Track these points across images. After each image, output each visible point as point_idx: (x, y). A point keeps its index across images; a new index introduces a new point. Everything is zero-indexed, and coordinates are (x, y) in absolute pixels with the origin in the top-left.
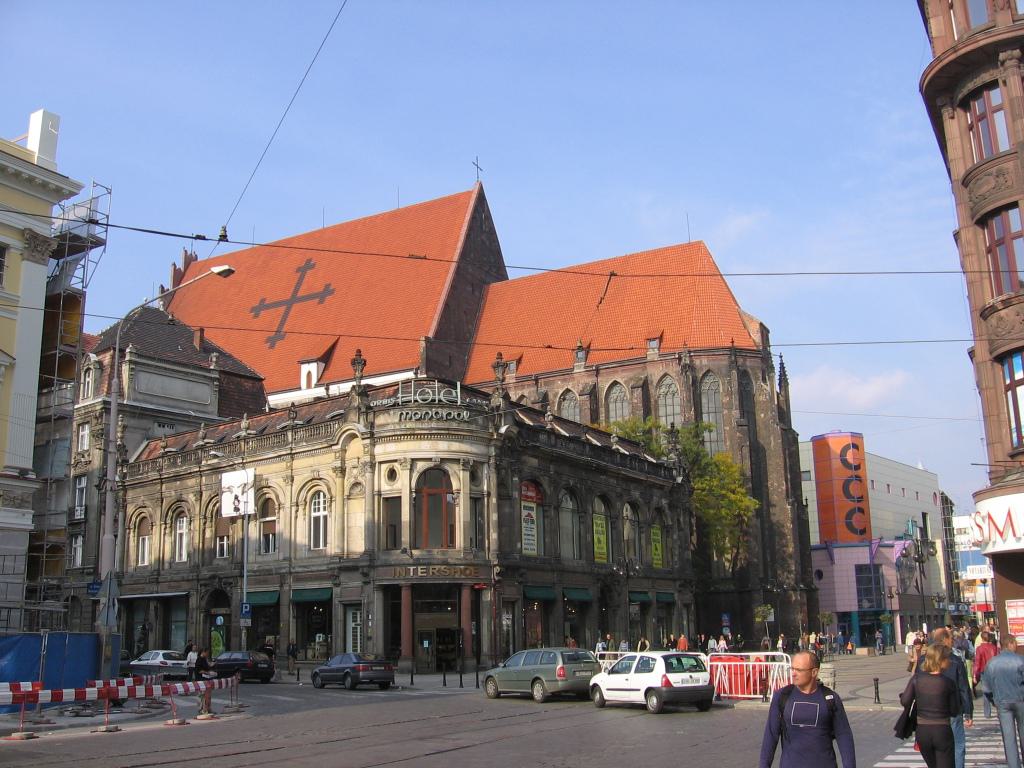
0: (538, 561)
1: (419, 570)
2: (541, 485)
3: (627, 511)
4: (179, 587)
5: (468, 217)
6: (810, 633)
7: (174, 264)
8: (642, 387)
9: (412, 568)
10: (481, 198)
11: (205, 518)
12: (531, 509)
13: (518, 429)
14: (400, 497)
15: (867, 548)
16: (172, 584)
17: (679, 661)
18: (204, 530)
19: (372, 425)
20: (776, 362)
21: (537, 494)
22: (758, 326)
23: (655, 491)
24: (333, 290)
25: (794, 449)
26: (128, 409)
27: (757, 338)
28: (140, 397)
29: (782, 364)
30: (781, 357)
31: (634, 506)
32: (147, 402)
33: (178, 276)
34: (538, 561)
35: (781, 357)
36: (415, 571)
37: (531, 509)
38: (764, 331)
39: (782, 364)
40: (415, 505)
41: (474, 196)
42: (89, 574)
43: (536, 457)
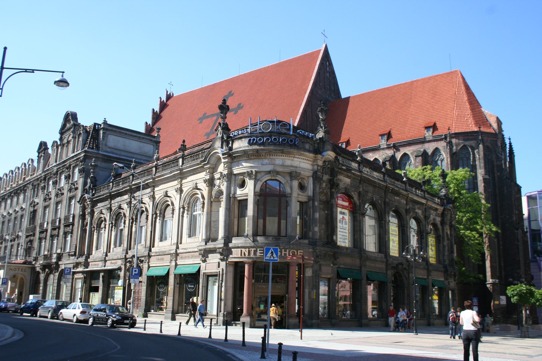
0: (349, 251)
1: (258, 251)
2: (353, 198)
3: (413, 224)
4: (116, 263)
5: (318, 63)
6: (339, 305)
7: (160, 98)
8: (422, 156)
9: (253, 249)
10: (326, 56)
11: (132, 219)
12: (344, 213)
13: (335, 155)
14: (247, 200)
15: (263, 330)
16: (113, 261)
17: (68, 226)
18: (132, 227)
19: (231, 149)
20: (507, 142)
21: (349, 204)
22: (495, 119)
23: (432, 212)
24: (243, 106)
25: (518, 196)
26: (100, 156)
27: (495, 126)
28: (108, 150)
29: (510, 143)
30: (510, 139)
31: (417, 219)
32: (113, 153)
33: (163, 106)
34: (349, 251)
35: (510, 139)
36: (255, 252)
37: (344, 213)
38: (499, 123)
39: (510, 143)
40: (257, 203)
41: (322, 52)
42: (72, 255)
43: (348, 177)
